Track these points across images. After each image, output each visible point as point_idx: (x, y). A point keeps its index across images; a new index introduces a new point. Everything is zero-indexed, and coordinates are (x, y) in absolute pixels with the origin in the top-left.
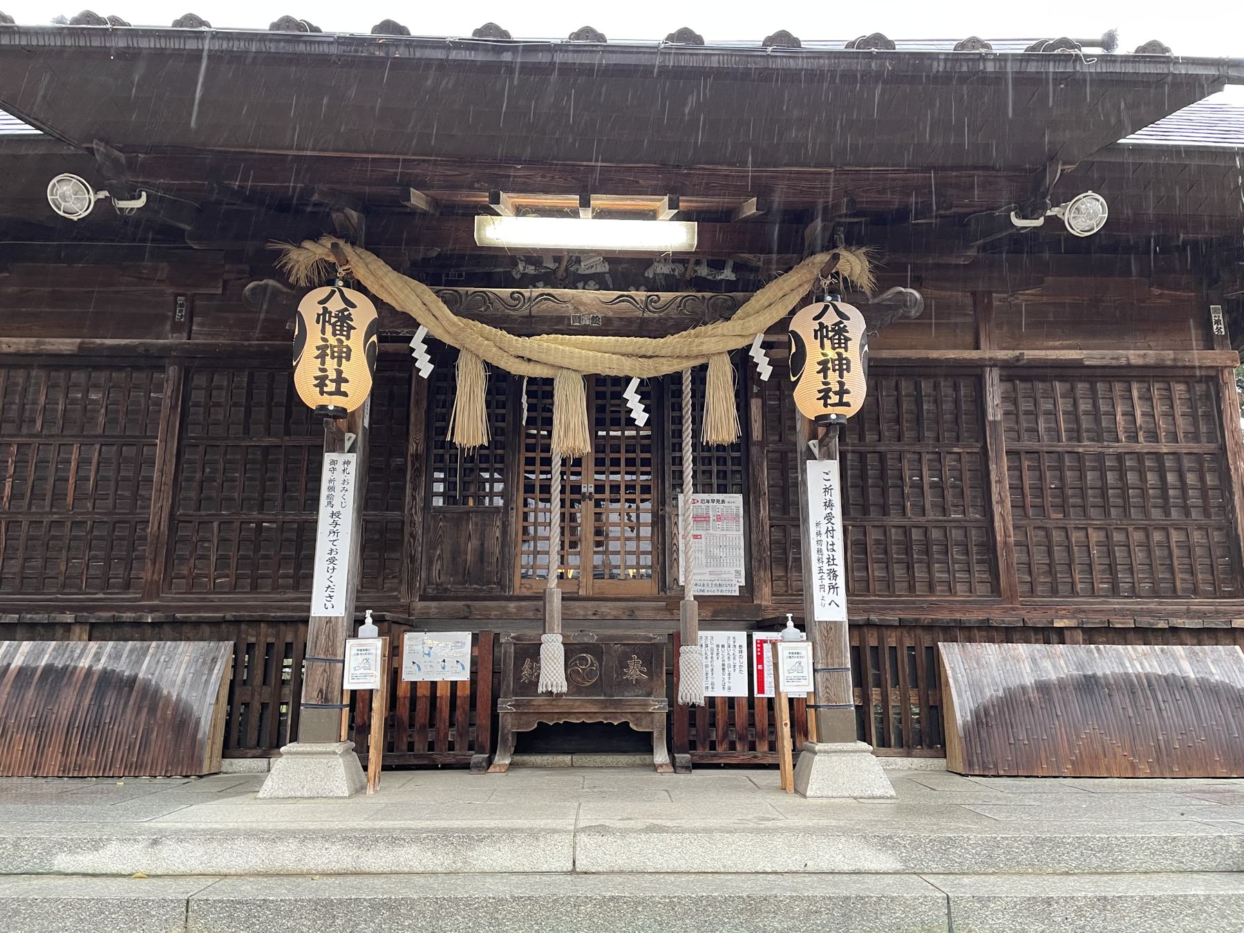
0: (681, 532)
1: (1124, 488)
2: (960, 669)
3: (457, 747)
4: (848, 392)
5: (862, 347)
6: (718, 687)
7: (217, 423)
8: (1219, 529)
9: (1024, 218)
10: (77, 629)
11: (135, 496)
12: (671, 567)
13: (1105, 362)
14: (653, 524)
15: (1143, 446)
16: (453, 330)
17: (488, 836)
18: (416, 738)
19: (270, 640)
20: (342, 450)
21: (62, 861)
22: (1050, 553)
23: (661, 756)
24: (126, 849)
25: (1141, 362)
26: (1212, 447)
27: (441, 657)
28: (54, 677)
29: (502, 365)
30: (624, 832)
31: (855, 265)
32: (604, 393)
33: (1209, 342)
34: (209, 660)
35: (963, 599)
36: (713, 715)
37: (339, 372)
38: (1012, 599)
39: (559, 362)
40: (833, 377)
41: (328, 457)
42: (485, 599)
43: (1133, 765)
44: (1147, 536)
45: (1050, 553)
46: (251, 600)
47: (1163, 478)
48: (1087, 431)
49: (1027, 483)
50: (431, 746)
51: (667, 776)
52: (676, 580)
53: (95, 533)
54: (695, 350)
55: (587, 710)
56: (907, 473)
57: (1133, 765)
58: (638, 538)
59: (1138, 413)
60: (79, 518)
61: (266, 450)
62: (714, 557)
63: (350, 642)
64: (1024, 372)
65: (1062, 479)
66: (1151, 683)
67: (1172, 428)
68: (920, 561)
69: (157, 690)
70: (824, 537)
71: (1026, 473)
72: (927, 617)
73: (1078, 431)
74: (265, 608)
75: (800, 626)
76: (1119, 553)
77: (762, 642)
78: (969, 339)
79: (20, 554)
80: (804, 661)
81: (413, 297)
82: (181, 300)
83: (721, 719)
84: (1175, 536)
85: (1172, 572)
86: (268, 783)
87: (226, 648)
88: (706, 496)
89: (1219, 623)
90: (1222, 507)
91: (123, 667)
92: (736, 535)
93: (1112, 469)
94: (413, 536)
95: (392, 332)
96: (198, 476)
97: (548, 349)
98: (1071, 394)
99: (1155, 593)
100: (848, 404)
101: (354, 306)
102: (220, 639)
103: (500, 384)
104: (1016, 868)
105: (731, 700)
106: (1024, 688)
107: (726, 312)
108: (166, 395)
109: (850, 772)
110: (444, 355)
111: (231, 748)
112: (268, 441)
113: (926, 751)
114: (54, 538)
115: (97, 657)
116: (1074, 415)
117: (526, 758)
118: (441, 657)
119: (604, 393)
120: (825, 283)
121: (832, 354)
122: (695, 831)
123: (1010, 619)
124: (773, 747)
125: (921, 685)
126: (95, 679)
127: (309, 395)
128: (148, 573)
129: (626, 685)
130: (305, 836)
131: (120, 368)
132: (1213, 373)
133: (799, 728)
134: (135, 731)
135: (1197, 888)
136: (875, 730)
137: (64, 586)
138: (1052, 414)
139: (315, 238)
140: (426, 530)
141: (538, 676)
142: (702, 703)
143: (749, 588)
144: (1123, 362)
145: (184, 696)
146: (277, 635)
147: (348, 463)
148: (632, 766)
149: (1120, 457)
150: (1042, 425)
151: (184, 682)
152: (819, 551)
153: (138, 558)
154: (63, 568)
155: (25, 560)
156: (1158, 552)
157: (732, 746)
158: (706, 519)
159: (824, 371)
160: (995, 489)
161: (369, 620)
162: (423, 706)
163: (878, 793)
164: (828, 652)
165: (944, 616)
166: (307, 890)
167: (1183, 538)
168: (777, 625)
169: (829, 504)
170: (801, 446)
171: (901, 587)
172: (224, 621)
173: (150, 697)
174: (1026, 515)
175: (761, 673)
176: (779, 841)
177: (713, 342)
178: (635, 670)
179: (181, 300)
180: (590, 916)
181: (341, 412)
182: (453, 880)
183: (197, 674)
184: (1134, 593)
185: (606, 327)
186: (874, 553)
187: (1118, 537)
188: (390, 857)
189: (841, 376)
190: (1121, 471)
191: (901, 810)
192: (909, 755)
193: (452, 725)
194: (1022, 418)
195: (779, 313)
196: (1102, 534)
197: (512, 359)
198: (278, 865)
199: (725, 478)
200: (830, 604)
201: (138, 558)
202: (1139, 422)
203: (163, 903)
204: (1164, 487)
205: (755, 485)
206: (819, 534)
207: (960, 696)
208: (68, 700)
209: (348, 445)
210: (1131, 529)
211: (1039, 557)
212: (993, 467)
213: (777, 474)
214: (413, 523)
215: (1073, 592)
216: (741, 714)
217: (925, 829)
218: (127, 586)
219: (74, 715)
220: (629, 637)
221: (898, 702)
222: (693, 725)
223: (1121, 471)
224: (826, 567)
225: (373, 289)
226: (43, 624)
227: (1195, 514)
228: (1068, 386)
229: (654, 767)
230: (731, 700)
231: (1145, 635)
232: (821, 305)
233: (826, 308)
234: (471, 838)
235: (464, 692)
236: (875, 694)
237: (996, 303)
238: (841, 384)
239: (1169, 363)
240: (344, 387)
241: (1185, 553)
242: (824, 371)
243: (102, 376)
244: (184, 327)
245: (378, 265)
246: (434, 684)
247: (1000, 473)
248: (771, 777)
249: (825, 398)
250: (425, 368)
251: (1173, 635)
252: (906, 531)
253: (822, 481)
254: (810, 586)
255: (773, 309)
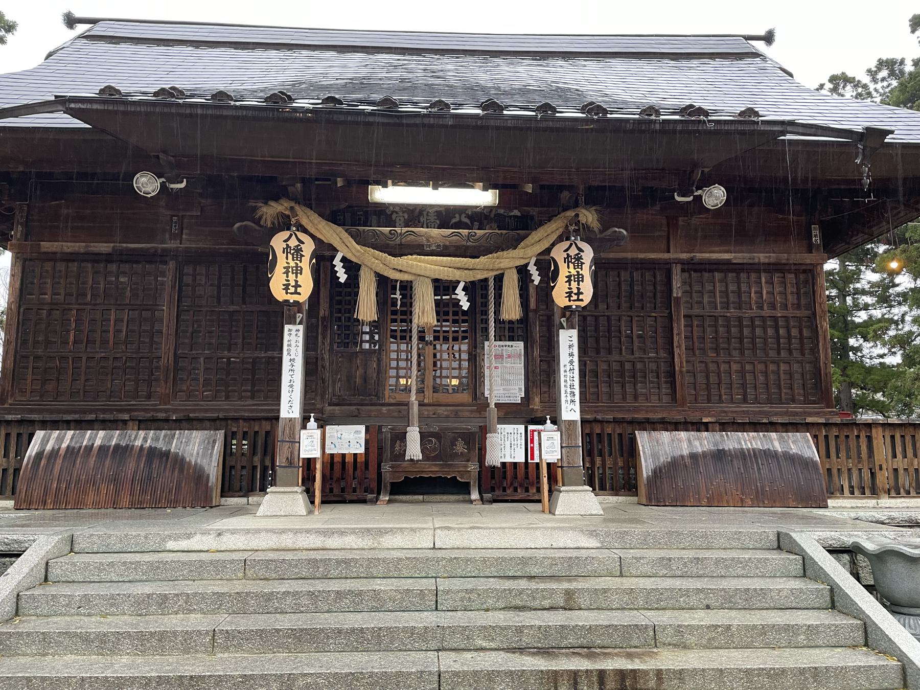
0: (487, 365)
1: (753, 339)
2: (647, 446)
3: (358, 490)
4: (582, 293)
5: (591, 267)
6: (508, 456)
7: (200, 297)
8: (810, 363)
9: (683, 196)
10: (131, 423)
11: (152, 342)
12: (480, 386)
13: (745, 261)
14: (469, 360)
15: (766, 312)
16: (358, 254)
17: (390, 531)
18: (334, 486)
19: (245, 430)
20: (295, 323)
21: (171, 545)
22: (707, 377)
23: (475, 495)
24: (204, 538)
25: (767, 261)
26: (808, 313)
27: (349, 439)
28: (121, 451)
29: (386, 274)
30: (459, 529)
31: (589, 217)
32: (443, 287)
33: (810, 248)
34: (211, 441)
35: (654, 403)
36: (505, 473)
37: (296, 282)
38: (683, 405)
39: (419, 272)
40: (574, 285)
41: (287, 327)
42: (367, 405)
43: (742, 500)
44: (766, 367)
45: (707, 377)
46: (225, 405)
47: (777, 332)
48: (733, 303)
49: (695, 334)
50: (343, 490)
51: (478, 506)
52: (483, 394)
53: (128, 364)
54: (497, 266)
55: (433, 470)
56: (623, 328)
57: (742, 500)
58: (460, 368)
59: (764, 292)
60: (118, 355)
61: (232, 313)
62: (506, 380)
63: (303, 432)
64: (697, 267)
65: (716, 332)
66: (756, 454)
67: (784, 301)
68: (629, 382)
69: (183, 458)
70: (568, 373)
71: (695, 328)
72: (628, 416)
73: (728, 303)
74: (236, 411)
75: (554, 422)
76: (749, 377)
77: (533, 431)
78: (663, 246)
79: (83, 378)
80: (555, 442)
81: (335, 236)
82: (175, 219)
83: (509, 474)
84: (783, 367)
85: (780, 388)
86: (261, 507)
87: (220, 434)
88: (501, 343)
89: (797, 420)
90: (812, 350)
91: (161, 445)
92: (519, 366)
93: (747, 326)
94: (324, 367)
95: (323, 257)
96: (190, 329)
97: (412, 265)
98: (724, 281)
99: (769, 401)
100: (582, 300)
101: (303, 243)
102: (216, 429)
103: (384, 284)
104: (657, 546)
105: (515, 464)
106: (682, 457)
107: (514, 244)
108: (168, 280)
109: (579, 501)
110: (352, 268)
111: (227, 490)
112: (232, 308)
113: (627, 492)
114: (103, 367)
115: (145, 440)
116: (725, 293)
117: (397, 497)
118: (349, 439)
119: (443, 287)
120: (572, 228)
121: (574, 272)
122: (496, 529)
123: (679, 418)
124: (539, 490)
125: (625, 455)
126: (146, 452)
127: (278, 291)
128: (161, 389)
129: (455, 456)
130: (296, 532)
131: (137, 262)
132: (811, 268)
133: (552, 479)
134: (172, 481)
135: (747, 555)
136: (598, 482)
137: (111, 396)
138: (713, 292)
139: (276, 199)
140: (331, 363)
141: (405, 451)
142: (499, 465)
143: (527, 399)
144: (756, 261)
145: (199, 461)
146: (249, 427)
147: (298, 330)
148: (458, 501)
149: (752, 319)
150: (706, 300)
151: (198, 454)
152: (566, 381)
153: (155, 380)
154: (109, 386)
155: (86, 381)
156: (772, 377)
157: (516, 490)
158: (501, 357)
159: (569, 281)
160: (676, 339)
161: (312, 419)
162: (337, 468)
163: (594, 512)
164: (569, 437)
165: (640, 416)
166: (304, 555)
167: (788, 368)
168: (542, 422)
169: (571, 355)
170: (557, 321)
171: (618, 397)
172: (218, 419)
173: (179, 462)
174: (694, 354)
175: (532, 449)
176: (538, 533)
177: (507, 261)
178: (460, 447)
179: (175, 219)
180: (445, 567)
181: (296, 303)
182: (373, 552)
183: (205, 449)
184: (756, 401)
185: (444, 251)
186: (602, 377)
187: (748, 367)
188: (340, 541)
189: (578, 284)
190: (753, 327)
191: (606, 520)
192: (616, 495)
193: (354, 478)
194: (694, 295)
195: (545, 245)
196: (739, 365)
197: (391, 271)
198: (283, 546)
199: (513, 332)
200: (571, 411)
201: (155, 380)
202: (764, 297)
203: (232, 562)
204: (778, 337)
205: (532, 336)
206: (565, 371)
207: (646, 461)
208: (131, 465)
209: (298, 320)
210: (756, 363)
211: (701, 379)
212: (675, 325)
213: (545, 329)
214: (323, 359)
215: (720, 401)
216: (521, 472)
217: (613, 528)
218: (149, 397)
219: (135, 473)
220: (457, 429)
221: (608, 462)
222: (493, 478)
223: (753, 327)
224: (569, 390)
225: (312, 231)
226: (110, 421)
227: (796, 354)
228: (722, 275)
229: (471, 502)
230: (515, 464)
231: (755, 426)
232: (568, 243)
233: (571, 245)
234: (381, 532)
235: (361, 460)
236: (598, 461)
237: (681, 223)
238: (579, 289)
239: (784, 261)
240: (299, 290)
241: (788, 377)
242: (569, 281)
243: (126, 267)
244: (178, 236)
245: (315, 217)
246: (344, 455)
247: (679, 328)
248: (538, 506)
249: (570, 296)
250: (343, 277)
251: (771, 427)
252: (622, 363)
253: (568, 341)
254: (560, 401)
255: (541, 243)
